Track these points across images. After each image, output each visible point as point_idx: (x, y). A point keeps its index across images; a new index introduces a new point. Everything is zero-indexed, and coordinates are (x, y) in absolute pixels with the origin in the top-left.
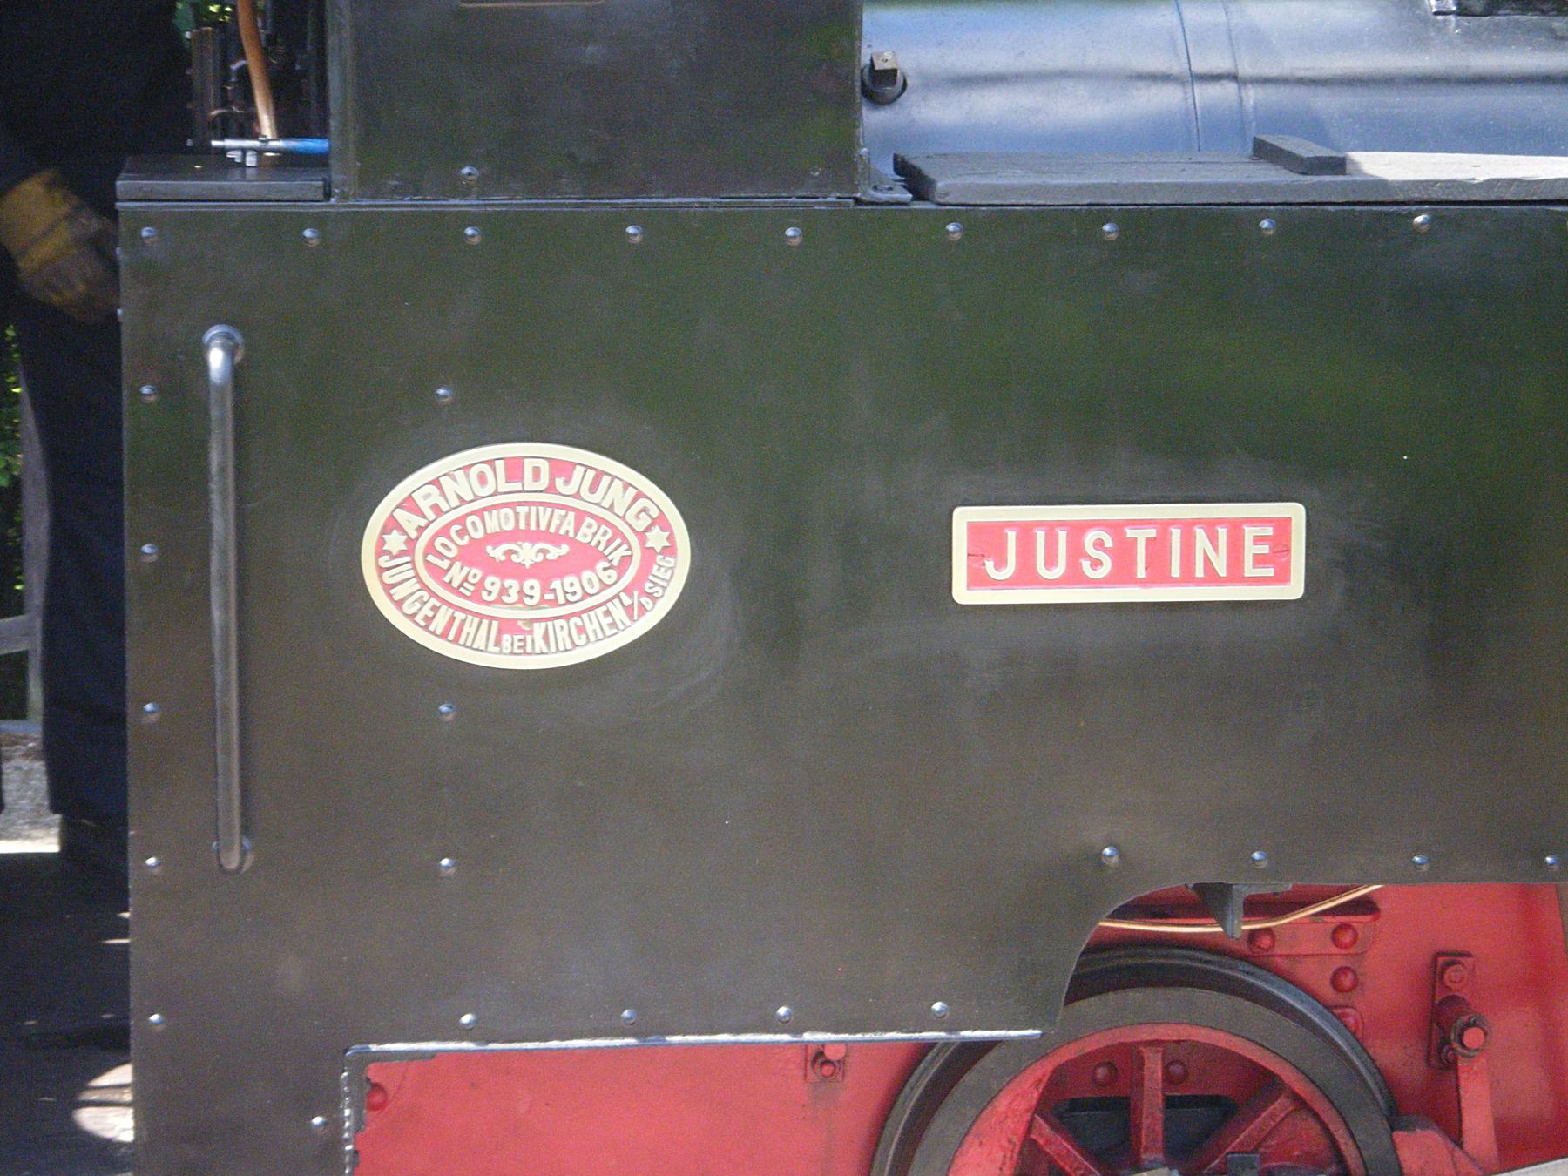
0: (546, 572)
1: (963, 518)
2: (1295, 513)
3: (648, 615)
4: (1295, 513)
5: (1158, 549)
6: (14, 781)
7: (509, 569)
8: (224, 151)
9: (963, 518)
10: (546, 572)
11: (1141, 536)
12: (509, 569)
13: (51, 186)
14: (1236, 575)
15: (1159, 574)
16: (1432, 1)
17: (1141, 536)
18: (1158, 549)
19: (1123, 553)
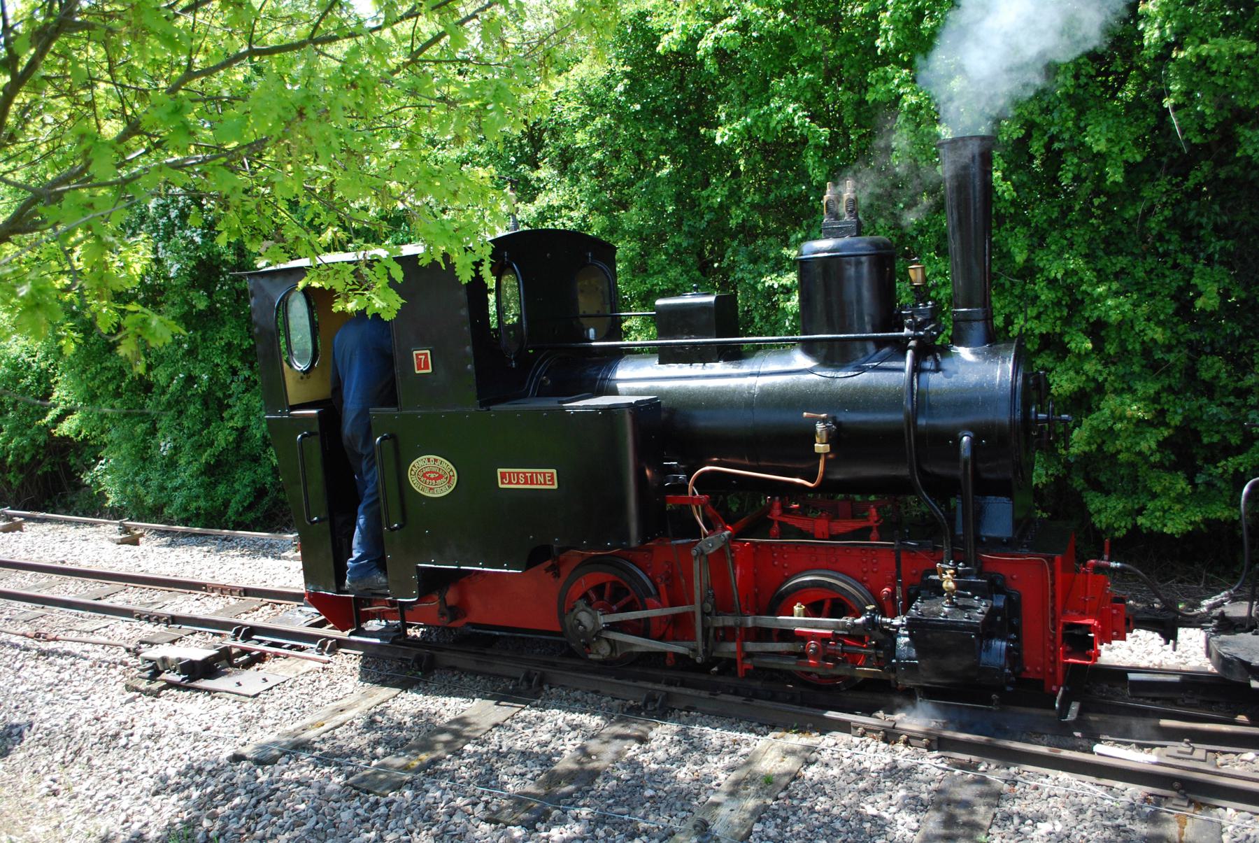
0: (436, 479)
10: (436, 479)
15: (532, 483)
19: (526, 478)
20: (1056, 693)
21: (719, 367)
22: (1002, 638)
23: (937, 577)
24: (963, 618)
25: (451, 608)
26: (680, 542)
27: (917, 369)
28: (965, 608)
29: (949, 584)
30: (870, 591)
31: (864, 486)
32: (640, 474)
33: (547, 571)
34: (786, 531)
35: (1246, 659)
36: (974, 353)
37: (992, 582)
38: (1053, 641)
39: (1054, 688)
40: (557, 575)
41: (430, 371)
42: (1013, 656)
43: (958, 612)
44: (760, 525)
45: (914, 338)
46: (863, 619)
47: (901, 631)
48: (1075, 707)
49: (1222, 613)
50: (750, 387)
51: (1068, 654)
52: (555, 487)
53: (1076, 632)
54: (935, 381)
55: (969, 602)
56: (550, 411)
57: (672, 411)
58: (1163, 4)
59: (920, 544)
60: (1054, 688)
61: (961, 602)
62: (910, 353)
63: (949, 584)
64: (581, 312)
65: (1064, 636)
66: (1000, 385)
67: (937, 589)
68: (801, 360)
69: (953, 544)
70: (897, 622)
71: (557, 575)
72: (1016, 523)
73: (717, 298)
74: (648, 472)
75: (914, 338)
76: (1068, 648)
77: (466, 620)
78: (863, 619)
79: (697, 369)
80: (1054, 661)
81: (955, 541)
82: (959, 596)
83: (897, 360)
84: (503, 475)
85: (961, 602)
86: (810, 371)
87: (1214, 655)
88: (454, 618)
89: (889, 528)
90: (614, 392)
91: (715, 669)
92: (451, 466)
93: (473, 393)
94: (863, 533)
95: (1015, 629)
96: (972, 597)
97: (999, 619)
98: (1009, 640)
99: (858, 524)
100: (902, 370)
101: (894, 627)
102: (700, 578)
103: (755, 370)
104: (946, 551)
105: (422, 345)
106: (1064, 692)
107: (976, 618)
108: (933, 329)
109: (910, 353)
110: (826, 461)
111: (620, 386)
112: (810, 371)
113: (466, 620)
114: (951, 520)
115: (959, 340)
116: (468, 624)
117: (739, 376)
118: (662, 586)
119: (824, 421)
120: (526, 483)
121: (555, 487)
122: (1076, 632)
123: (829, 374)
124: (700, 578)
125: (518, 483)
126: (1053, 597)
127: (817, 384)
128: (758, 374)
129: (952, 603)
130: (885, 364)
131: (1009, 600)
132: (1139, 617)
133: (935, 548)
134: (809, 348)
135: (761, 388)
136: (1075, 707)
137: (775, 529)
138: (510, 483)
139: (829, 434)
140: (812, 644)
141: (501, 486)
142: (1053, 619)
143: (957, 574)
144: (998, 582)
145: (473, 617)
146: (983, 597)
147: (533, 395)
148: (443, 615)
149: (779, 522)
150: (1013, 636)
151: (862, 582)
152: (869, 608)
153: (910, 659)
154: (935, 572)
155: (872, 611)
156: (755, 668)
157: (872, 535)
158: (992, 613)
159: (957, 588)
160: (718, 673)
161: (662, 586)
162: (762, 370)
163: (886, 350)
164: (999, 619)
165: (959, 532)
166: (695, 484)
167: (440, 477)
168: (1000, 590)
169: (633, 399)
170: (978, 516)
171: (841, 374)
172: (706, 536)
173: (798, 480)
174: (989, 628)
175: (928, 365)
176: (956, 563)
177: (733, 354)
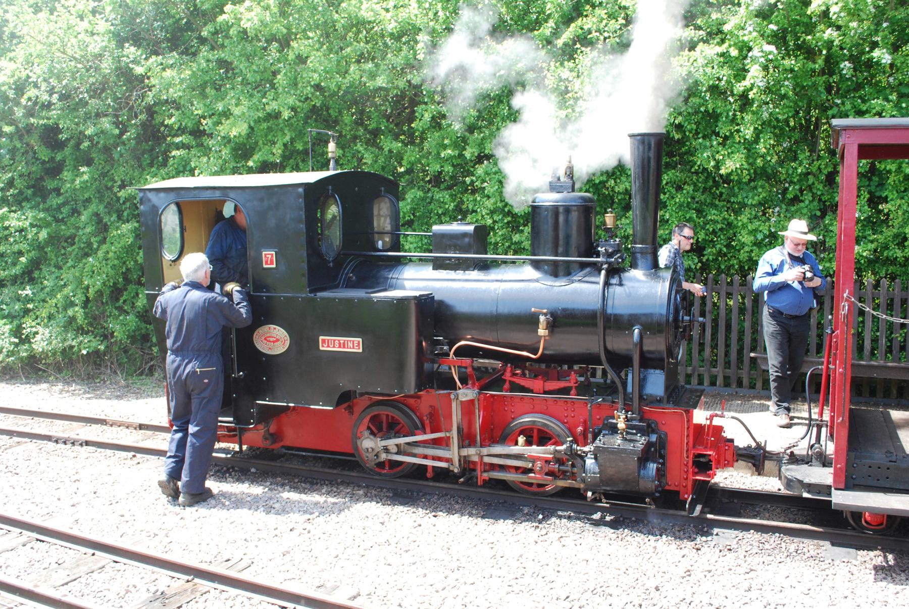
0: (274, 342)
1: (321, 338)
2: (360, 340)
3: (634, 399)
4: (360, 340)
5: (344, 344)
6: (821, 414)
7: (270, 341)
8: (640, 421)
9: (321, 338)
10: (274, 342)
11: (342, 342)
12: (270, 341)
13: (661, 315)
14: (353, 348)
15: (344, 347)
16: (817, 1)
17: (342, 342)
18: (344, 344)
19: (340, 344)
20: (687, 499)
21: (474, 274)
22: (654, 462)
23: (614, 421)
24: (630, 446)
25: (272, 435)
26: (442, 392)
27: (607, 284)
28: (631, 441)
29: (621, 425)
30: (570, 429)
31: (570, 360)
32: (419, 344)
33: (345, 409)
34: (515, 387)
35: (801, 479)
36: (644, 275)
37: (649, 426)
38: (686, 465)
39: (686, 496)
40: (351, 413)
41: (274, 266)
42: (660, 473)
43: (627, 443)
44: (496, 382)
45: (607, 263)
46: (564, 447)
47: (589, 456)
48: (699, 508)
49: (792, 453)
50: (495, 290)
51: (695, 474)
52: (361, 350)
53: (702, 460)
54: (616, 291)
55: (634, 437)
56: (361, 300)
57: (441, 303)
58: (154, 3)
59: (603, 399)
60: (686, 496)
61: (629, 437)
62: (603, 272)
63: (621, 425)
64: (376, 229)
65: (694, 463)
66: (660, 296)
67: (614, 429)
68: (529, 272)
69: (625, 400)
70: (586, 449)
71: (351, 413)
72: (667, 388)
73: (476, 228)
74: (424, 344)
75: (607, 263)
76: (696, 470)
77: (281, 444)
78: (564, 447)
79: (459, 274)
80: (686, 479)
81: (627, 398)
82: (628, 433)
83: (594, 276)
84: (324, 341)
85: (629, 437)
86: (537, 281)
87: (783, 478)
88: (274, 442)
89: (584, 389)
90: (403, 288)
91: (462, 480)
92: (285, 333)
93: (305, 280)
94: (565, 391)
95: (662, 457)
96: (636, 434)
97: (653, 449)
98: (659, 463)
99: (562, 384)
100: (597, 283)
101: (584, 452)
102: (456, 416)
103: (499, 277)
104: (620, 406)
105: (269, 247)
106: (692, 498)
107: (638, 447)
108: (619, 257)
109: (603, 272)
110: (545, 340)
111: (407, 284)
112: (537, 281)
113: (281, 444)
114: (624, 384)
115: (634, 265)
116: (283, 447)
117: (488, 281)
118: (427, 422)
119: (545, 314)
120: (340, 347)
121: (361, 350)
122: (702, 460)
123: (550, 283)
124: (456, 416)
125: (334, 347)
126: (688, 436)
127: (541, 289)
128: (501, 281)
129: (623, 437)
130: (587, 279)
131: (659, 438)
132: (740, 452)
133: (613, 402)
134: (536, 265)
135: (503, 290)
136: (699, 508)
137: (507, 386)
138: (328, 346)
139: (548, 323)
140: (539, 464)
141: (321, 348)
142: (687, 451)
143: (627, 420)
144: (653, 425)
145: (287, 442)
146: (643, 435)
147: (342, 287)
148: (266, 439)
149: (510, 381)
150: (661, 461)
151: (563, 423)
152: (568, 439)
153: (594, 473)
154: (613, 418)
155: (571, 442)
156: (490, 479)
157: (572, 392)
158: (649, 445)
159: (627, 428)
160: (463, 483)
161: (427, 422)
162: (504, 279)
163: (588, 270)
164: (653, 449)
165: (629, 389)
166: (454, 354)
167: (277, 340)
168: (653, 432)
169: (417, 294)
170: (642, 383)
171: (558, 284)
172: (460, 389)
173: (525, 353)
174: (645, 457)
175: (614, 281)
176: (627, 412)
177: (484, 266)
